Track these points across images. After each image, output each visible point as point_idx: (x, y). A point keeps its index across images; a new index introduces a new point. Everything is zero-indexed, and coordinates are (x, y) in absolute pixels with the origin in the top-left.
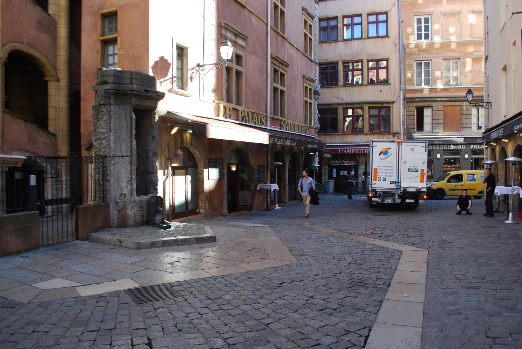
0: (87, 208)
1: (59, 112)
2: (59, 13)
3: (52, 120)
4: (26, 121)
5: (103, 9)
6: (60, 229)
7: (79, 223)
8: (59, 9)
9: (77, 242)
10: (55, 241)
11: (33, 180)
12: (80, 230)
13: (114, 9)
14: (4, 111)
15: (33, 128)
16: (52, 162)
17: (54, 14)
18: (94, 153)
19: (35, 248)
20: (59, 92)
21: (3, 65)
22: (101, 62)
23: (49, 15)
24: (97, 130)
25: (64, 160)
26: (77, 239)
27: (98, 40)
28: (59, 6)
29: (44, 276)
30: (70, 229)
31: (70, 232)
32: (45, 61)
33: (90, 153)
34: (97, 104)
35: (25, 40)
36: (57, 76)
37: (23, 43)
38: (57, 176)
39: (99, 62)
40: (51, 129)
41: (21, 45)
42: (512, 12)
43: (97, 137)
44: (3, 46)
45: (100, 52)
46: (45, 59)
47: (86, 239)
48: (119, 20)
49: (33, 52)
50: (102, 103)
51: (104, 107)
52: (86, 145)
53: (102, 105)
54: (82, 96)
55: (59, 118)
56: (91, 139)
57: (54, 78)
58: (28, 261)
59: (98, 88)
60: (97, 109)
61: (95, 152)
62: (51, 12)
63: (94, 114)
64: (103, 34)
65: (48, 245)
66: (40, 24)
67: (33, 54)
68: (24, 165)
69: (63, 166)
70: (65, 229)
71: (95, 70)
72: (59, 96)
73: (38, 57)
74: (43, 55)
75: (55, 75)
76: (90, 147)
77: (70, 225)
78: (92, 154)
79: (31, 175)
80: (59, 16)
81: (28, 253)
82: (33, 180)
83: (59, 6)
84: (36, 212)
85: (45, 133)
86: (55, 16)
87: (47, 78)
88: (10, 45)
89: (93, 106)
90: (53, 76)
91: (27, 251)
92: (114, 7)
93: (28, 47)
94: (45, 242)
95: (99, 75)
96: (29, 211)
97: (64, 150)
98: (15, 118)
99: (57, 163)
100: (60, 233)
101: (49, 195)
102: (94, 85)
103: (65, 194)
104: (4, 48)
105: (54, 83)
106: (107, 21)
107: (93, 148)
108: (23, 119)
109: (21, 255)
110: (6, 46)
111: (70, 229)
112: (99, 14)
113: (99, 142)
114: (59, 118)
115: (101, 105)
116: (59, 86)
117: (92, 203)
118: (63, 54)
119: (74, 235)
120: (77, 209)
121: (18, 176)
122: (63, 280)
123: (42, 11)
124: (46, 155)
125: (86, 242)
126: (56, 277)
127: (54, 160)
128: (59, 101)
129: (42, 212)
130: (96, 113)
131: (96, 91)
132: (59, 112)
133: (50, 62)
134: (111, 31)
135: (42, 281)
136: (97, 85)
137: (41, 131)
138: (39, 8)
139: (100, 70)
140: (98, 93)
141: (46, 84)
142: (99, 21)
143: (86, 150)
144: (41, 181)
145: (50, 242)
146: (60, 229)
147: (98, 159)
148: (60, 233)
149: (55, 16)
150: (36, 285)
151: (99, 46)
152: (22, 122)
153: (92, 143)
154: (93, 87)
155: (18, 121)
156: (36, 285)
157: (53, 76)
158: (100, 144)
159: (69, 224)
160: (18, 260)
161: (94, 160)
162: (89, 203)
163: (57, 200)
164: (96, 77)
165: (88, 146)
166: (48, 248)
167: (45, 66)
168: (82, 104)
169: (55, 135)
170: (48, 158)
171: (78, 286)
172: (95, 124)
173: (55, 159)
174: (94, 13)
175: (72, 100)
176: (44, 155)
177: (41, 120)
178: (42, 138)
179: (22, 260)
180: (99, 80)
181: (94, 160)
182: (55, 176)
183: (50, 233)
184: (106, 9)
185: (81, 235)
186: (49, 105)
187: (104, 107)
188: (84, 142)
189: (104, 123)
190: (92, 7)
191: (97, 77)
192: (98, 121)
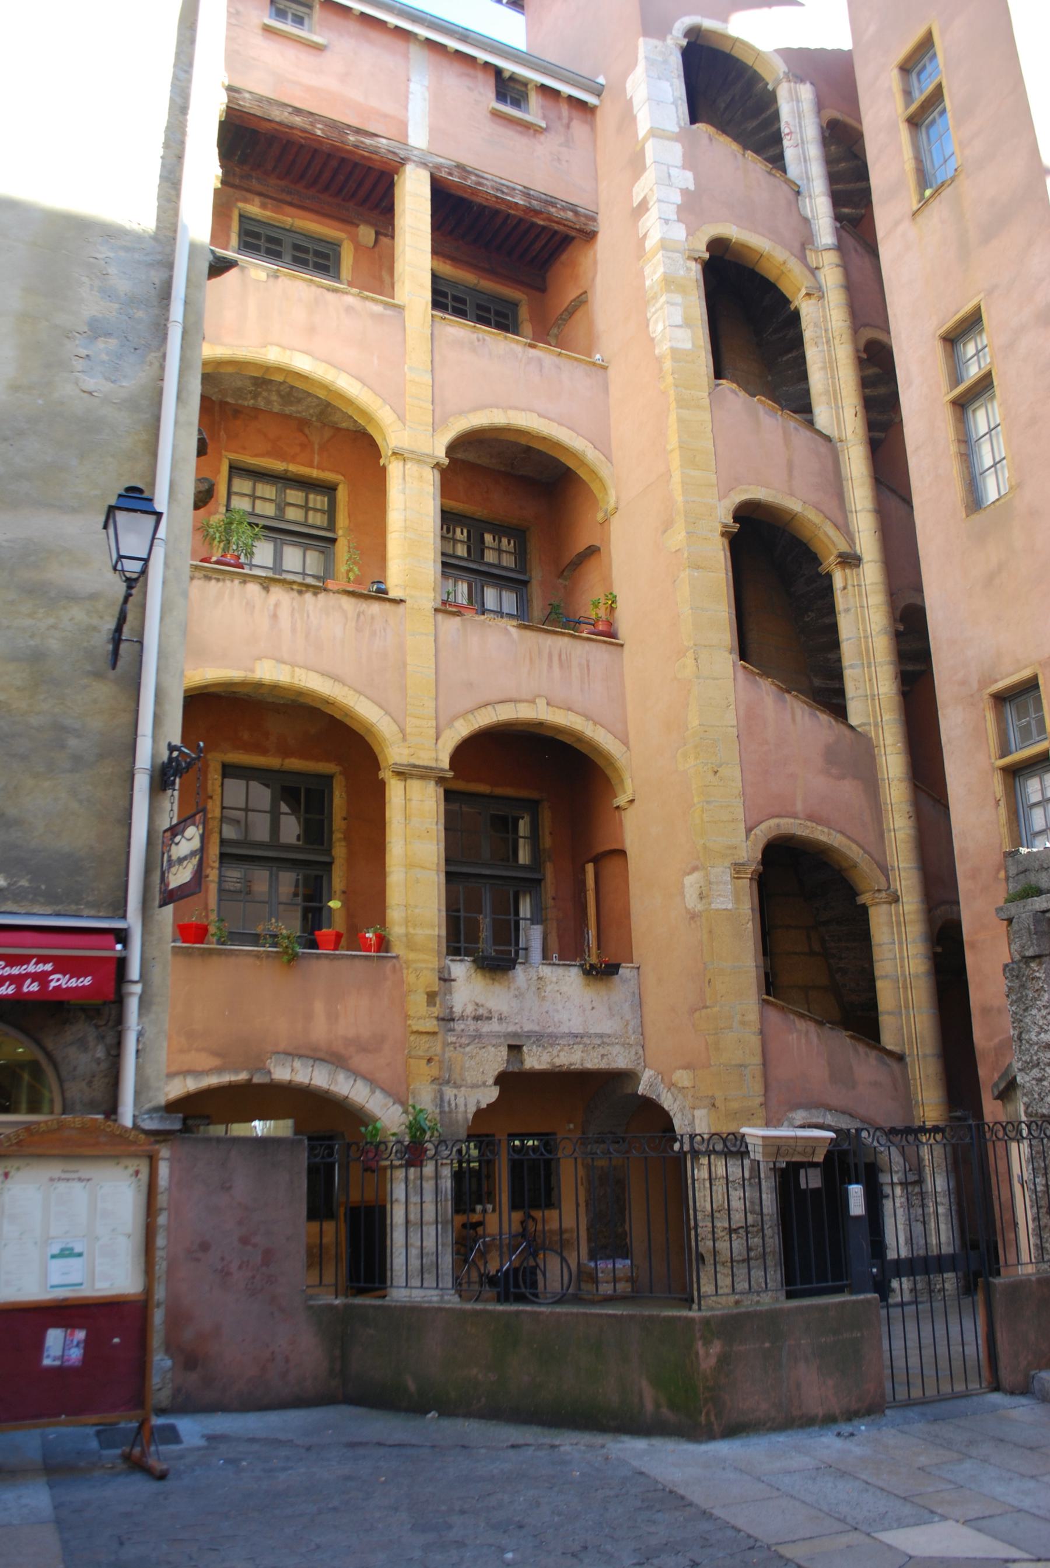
0: (1017, 1288)
1: (905, 988)
2: (875, 717)
3: (889, 1013)
4: (820, 1023)
5: (996, 681)
6: (942, 1350)
7: (998, 1335)
8: (873, 705)
9: (996, 1398)
10: (931, 1392)
11: (856, 1196)
12: (1003, 1360)
13: (1026, 674)
14: (764, 1000)
15: (842, 1039)
16: (904, 1143)
17: (864, 724)
18: (1022, 1108)
19: (871, 1409)
20: (899, 933)
21: (751, 879)
22: (1011, 831)
23: (851, 727)
24: (1025, 1036)
25: (939, 1137)
26: (996, 1388)
27: (994, 769)
28: (873, 699)
29: (907, 1510)
30: (971, 1350)
31: (971, 1363)
32: (854, 852)
33: (1010, 1108)
34: (1017, 957)
35: (799, 807)
36: (889, 887)
37: (794, 816)
38: (914, 1181)
39: (1004, 830)
40: (889, 1040)
41: (792, 820)
42: (111, 569)
43: (1027, 1058)
44: (749, 831)
45: (1002, 803)
46: (854, 846)
47: (1024, 1389)
48: (1045, 702)
49: (821, 834)
50: (1029, 953)
51: (1040, 964)
52: (996, 1085)
53: (1033, 958)
54: (966, 937)
55: (907, 1007)
56: (1010, 1065)
57: (883, 895)
58: (858, 1451)
59: (1013, 909)
60: (1017, 972)
61: (1027, 1106)
62: (853, 720)
63: (1010, 988)
64: (1004, 752)
65: (909, 1403)
66: (831, 756)
67: (823, 838)
68: (829, 1155)
69: (932, 1153)
70: (940, 1327)
71: (997, 858)
72: (900, 943)
73: (836, 844)
74: (849, 837)
75: (883, 885)
76: (1008, 1090)
77: (969, 1337)
78: (1016, 1111)
79: (850, 1183)
80: (876, 725)
81: (856, 1422)
82: (856, 1196)
83: (873, 699)
84: (869, 1296)
85: (873, 1054)
86: (867, 728)
87: (864, 899)
88: (763, 826)
89: (1006, 966)
90: (879, 891)
91: (850, 1416)
92: (1025, 667)
93: (809, 823)
94: (901, 1394)
95: (1013, 871)
96: (852, 1293)
97: (930, 1105)
98: (792, 1017)
99: (919, 1144)
100: (943, 1364)
101: (897, 1243)
102: (1001, 903)
103: (942, 1237)
104: (752, 837)
105: (884, 908)
106: (1010, 711)
107: (1019, 1093)
108: (811, 1019)
109: (836, 1428)
110: (756, 831)
111: (971, 1350)
112: (987, 696)
113: (1036, 1073)
114: (907, 1007)
115: (1027, 960)
116: (897, 914)
117: (1030, 1269)
118: (899, 825)
119: (985, 1372)
120: (988, 1289)
121: (811, 1180)
122: (965, 1530)
123: (833, 722)
124: (887, 1125)
125: (1023, 1401)
126: (944, 1518)
127: (911, 1138)
128: (902, 959)
129: (883, 1289)
130: (1016, 984)
131: (1010, 921)
132: (905, 988)
133: (866, 852)
134: (1026, 734)
135: (901, 1523)
136: (1007, 901)
137: (862, 1049)
138: (824, 718)
139: (1013, 854)
140: (1015, 926)
141: (864, 910)
142: (990, 716)
143: (997, 1098)
144: (874, 1198)
145: (916, 1393)
146: (942, 1350)
147: (1040, 1128)
148: (943, 1364)
149: (867, 728)
150: (889, 1537)
151: (997, 785)
152: (812, 1027)
153: (1015, 1078)
154: (999, 910)
155: (801, 1025)
156: (889, 1537)
157: (879, 891)
158: (1040, 1080)
159: (964, 1334)
160: (827, 1444)
161: (1025, 1133)
162: (1022, 1271)
163: (926, 1259)
164: (1002, 874)
165: (1002, 1086)
166: (911, 1413)
167: (855, 866)
168: (970, 959)
169: (900, 1058)
170: (893, 1131)
171: (1014, 1561)
172: (1017, 1020)
173: (908, 1133)
174: (972, 696)
175: (939, 950)
176: (883, 1124)
177: (857, 1015)
178: (866, 1067)
179: (839, 1443)
180: (1013, 887)
181: (1025, 1133)
182: (912, 1178)
183: (914, 1361)
184: (1002, 679)
185: (1006, 1376)
186: (878, 973)
187: (1040, 964)
188: (987, 1075)
189: (1044, 1012)
190: (963, 683)
191: (1007, 878)
192: (1026, 1010)
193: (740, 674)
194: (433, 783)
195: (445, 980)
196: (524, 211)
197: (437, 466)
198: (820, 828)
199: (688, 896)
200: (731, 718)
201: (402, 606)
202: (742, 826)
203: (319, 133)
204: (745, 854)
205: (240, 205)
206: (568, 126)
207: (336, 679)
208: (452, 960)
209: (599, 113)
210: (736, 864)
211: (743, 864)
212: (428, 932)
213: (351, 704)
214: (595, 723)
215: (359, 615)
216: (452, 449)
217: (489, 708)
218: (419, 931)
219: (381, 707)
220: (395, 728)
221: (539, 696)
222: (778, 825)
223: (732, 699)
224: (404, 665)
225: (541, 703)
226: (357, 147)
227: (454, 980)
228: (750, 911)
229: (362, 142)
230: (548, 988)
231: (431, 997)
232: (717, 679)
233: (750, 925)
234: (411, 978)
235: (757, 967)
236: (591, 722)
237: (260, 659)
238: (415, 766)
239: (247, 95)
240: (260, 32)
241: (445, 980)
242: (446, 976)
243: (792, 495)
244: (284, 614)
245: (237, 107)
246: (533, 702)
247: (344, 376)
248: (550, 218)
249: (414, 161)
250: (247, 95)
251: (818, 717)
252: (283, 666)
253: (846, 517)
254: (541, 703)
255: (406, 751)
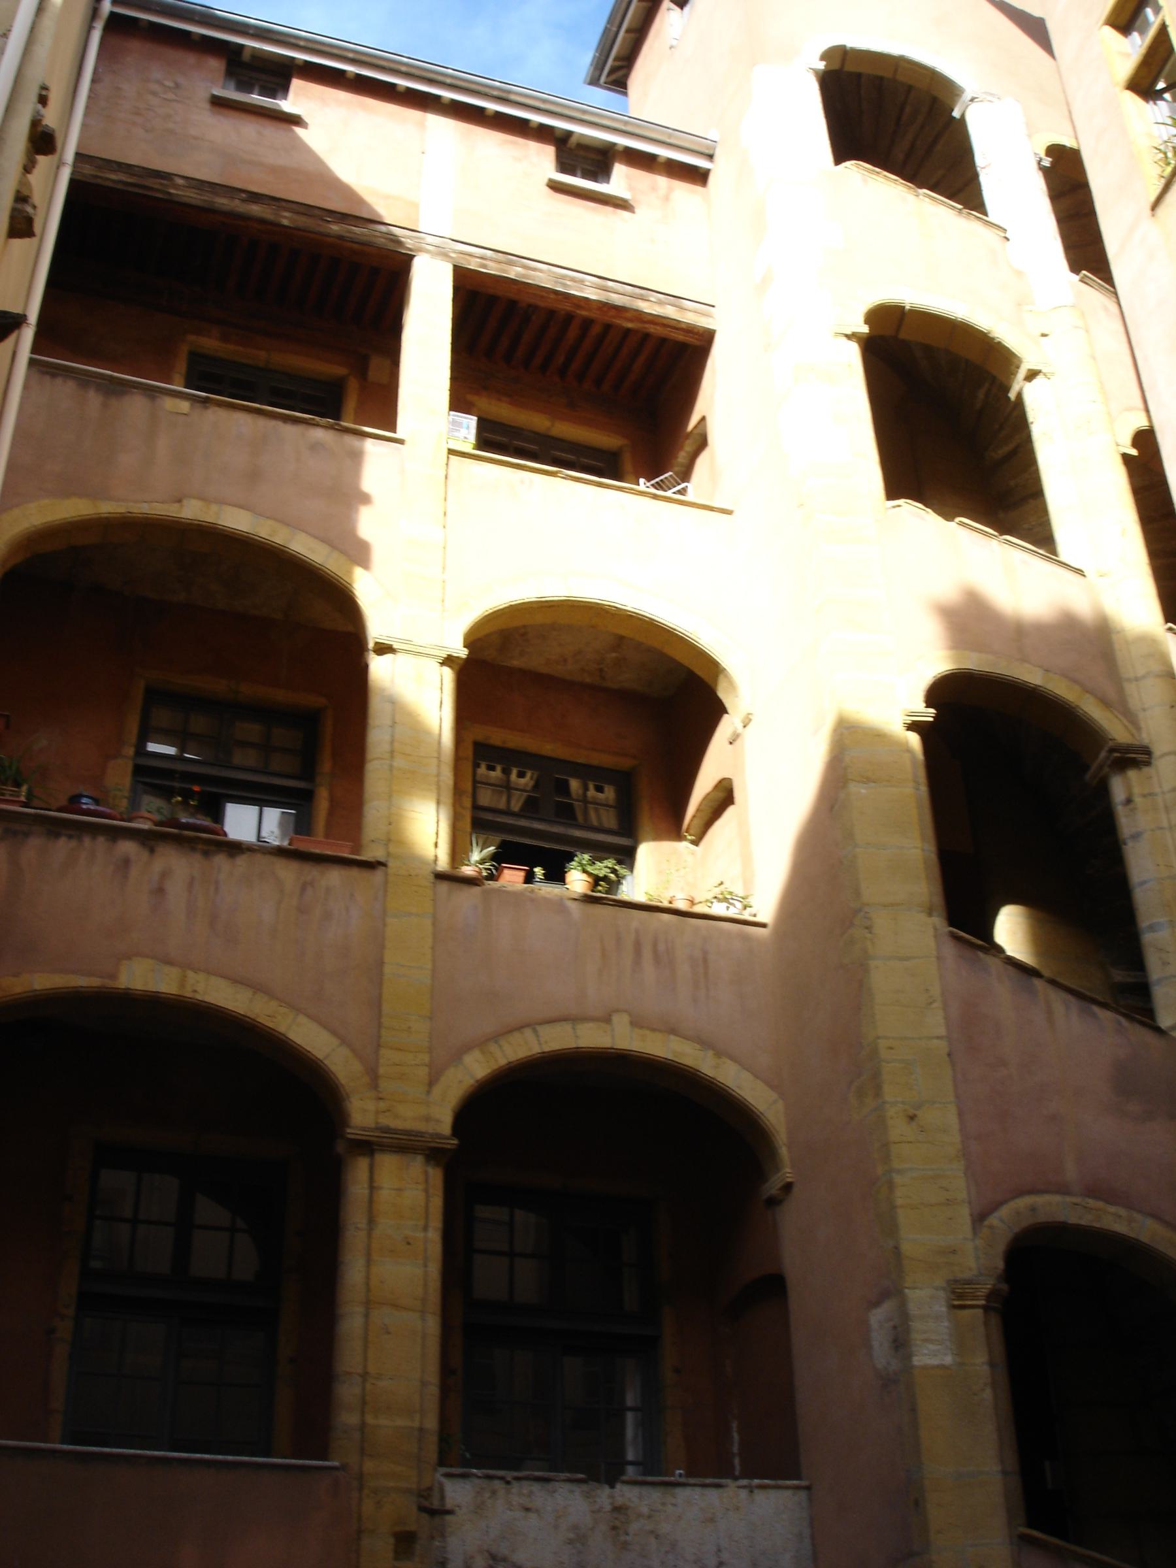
14: (1023, 1538)
35: (1071, 1172)
37: (1062, 1189)
41: (1057, 1198)
44: (979, 1219)
49: (1114, 1220)
66: (1126, 1082)
67: (1120, 1228)
73: (1144, 1238)
88: (1004, 1211)
93: (1091, 1202)
110: (993, 1220)
193: (950, 949)
194: (420, 1159)
195: (432, 1512)
196: (599, 309)
197: (448, 661)
198: (1112, 1209)
199: (875, 1344)
200: (936, 1024)
201: (378, 876)
202: (965, 1213)
203: (285, 222)
204: (972, 1263)
205: (192, 338)
206: (667, 198)
207: (258, 988)
208: (448, 1475)
209: (712, 179)
210: (956, 1281)
211: (969, 1282)
212: (400, 1422)
213: (282, 1029)
214: (719, 1054)
215: (303, 889)
216: (474, 640)
217: (528, 1032)
218: (383, 1422)
219: (334, 1033)
220: (357, 1066)
221: (617, 1011)
222: (1033, 1209)
223: (936, 991)
224: (381, 963)
225: (621, 1022)
226: (341, 238)
227: (450, 1512)
228: (986, 1368)
229: (350, 232)
230: (634, 1527)
231: (405, 1542)
232: (908, 959)
233: (988, 1394)
234: (368, 1507)
235: (1004, 1473)
236: (710, 1053)
237: (129, 958)
238: (387, 1130)
239: (180, 182)
240: (207, 106)
241: (432, 1512)
242: (436, 1504)
243: (1024, 660)
244: (176, 889)
245: (166, 197)
246: (607, 1020)
247: (302, 536)
248: (639, 315)
249: (428, 252)
250: (180, 182)
251: (1094, 1015)
252: (167, 969)
253: (1121, 691)
254: (621, 1022)
255: (371, 1106)
